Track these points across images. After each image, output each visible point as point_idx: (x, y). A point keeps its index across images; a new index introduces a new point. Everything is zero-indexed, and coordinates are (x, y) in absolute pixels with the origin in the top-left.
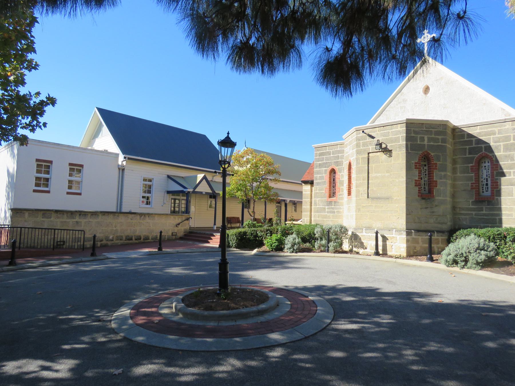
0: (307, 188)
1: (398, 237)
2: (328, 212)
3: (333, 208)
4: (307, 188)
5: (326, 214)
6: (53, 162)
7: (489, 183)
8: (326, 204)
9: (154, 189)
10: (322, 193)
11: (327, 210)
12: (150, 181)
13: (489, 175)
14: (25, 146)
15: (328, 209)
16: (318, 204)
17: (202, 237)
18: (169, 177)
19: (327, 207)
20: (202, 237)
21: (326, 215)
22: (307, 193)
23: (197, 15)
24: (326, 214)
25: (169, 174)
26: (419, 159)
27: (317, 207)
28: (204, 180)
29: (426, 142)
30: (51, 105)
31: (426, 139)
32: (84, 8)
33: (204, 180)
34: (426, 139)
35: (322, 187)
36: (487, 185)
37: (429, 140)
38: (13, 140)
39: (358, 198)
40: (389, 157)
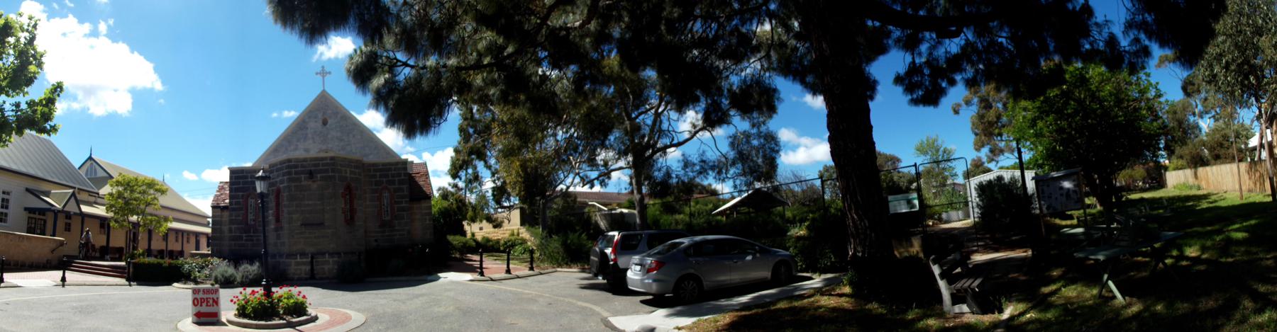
1: (331, 260)
2: (246, 240)
3: (251, 236)
6: (929, 110)
7: (389, 210)
9: (11, 205)
11: (244, 238)
12: (8, 194)
14: (35, 80)
18: (28, 190)
23: (705, 23)
25: (28, 187)
26: (609, 178)
28: (73, 198)
29: (348, 175)
31: (348, 172)
33: (73, 198)
34: (348, 172)
36: (387, 211)
37: (351, 172)
38: (1133, 61)
39: (218, 227)
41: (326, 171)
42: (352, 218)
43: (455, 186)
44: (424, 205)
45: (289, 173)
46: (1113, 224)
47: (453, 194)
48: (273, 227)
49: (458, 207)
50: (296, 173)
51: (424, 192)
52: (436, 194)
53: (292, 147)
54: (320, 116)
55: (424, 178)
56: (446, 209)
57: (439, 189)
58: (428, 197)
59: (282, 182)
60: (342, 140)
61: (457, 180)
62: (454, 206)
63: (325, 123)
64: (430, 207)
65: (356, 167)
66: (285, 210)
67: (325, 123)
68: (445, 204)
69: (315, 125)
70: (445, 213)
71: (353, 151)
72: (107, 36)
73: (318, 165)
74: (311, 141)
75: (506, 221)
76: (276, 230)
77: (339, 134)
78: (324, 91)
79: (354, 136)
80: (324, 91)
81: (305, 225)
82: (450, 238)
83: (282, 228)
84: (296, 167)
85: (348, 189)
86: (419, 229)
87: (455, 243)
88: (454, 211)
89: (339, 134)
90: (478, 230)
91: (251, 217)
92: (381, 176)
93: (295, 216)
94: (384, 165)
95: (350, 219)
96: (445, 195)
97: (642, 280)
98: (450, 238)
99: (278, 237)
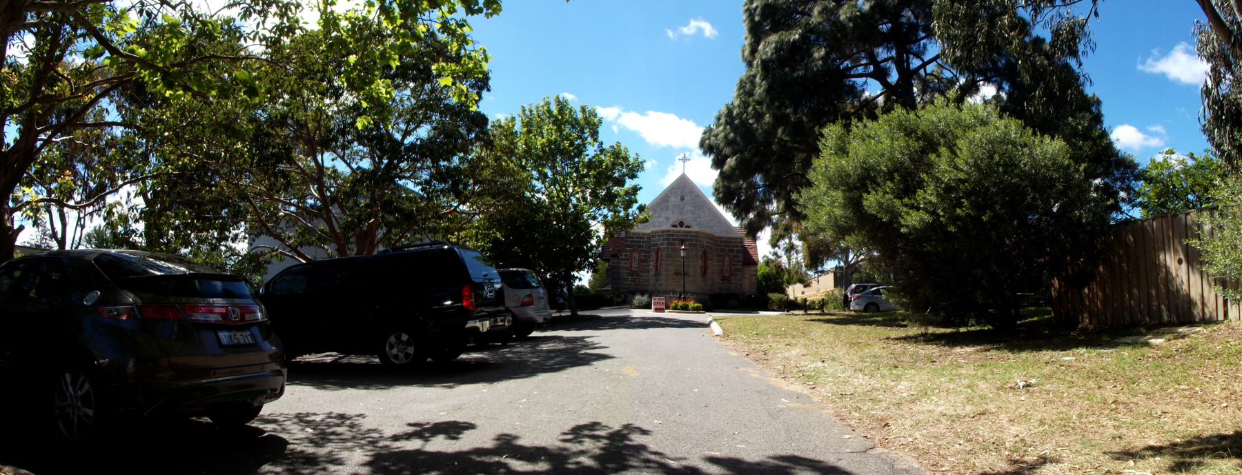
41: (692, 240)
42: (705, 272)
43: (775, 254)
44: (753, 268)
45: (668, 239)
46: (517, 253)
47: (773, 261)
48: (652, 273)
49: (777, 272)
50: (673, 240)
51: (753, 260)
52: (761, 260)
53: (657, 215)
54: (679, 193)
55: (753, 250)
56: (768, 274)
57: (764, 257)
58: (755, 263)
59: (662, 244)
60: (694, 213)
61: (777, 249)
62: (774, 271)
63: (682, 199)
64: (756, 271)
65: (710, 239)
66: (664, 263)
67: (682, 199)
68: (767, 270)
69: (674, 200)
70: (767, 277)
71: (716, 231)
72: (742, 239)
73: (687, 236)
74: (670, 212)
75: (133, 194)
76: (656, 275)
77: (692, 209)
78: (684, 174)
79: (704, 211)
80: (684, 174)
81: (677, 273)
82: (770, 295)
83: (660, 275)
84: (673, 235)
85: (705, 253)
86: (747, 285)
87: (773, 298)
88: (775, 276)
89: (692, 209)
90: (795, 292)
91: (634, 265)
92: (725, 246)
93: (670, 268)
94: (728, 238)
95: (704, 273)
96: (768, 263)
97: (741, 224)
98: (770, 295)
99: (657, 280)
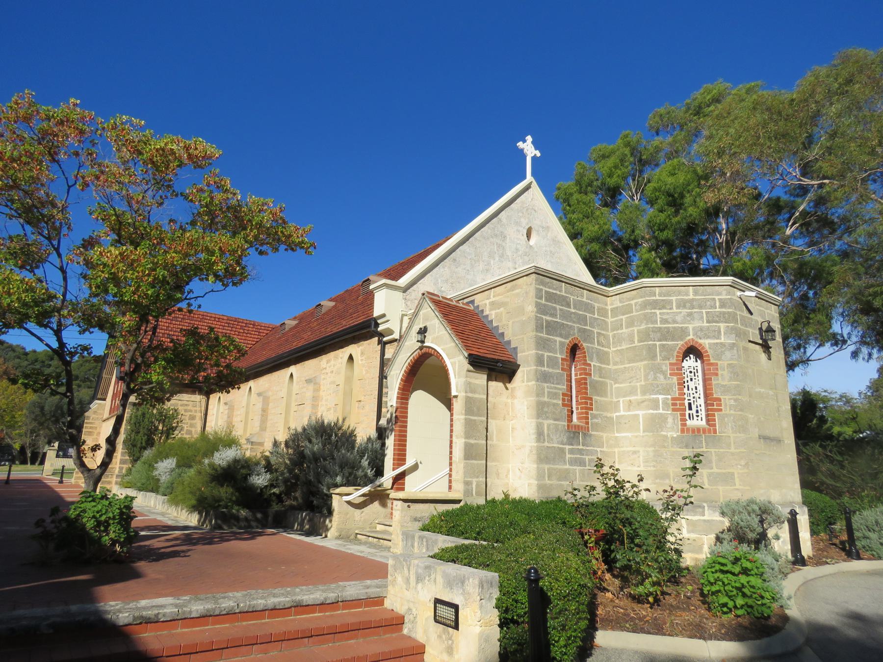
0: (478, 382)
2: (571, 464)
3: (580, 452)
4: (478, 382)
5: (567, 466)
8: (565, 440)
10: (554, 405)
11: (568, 456)
13: (749, 91)
15: (571, 452)
16: (548, 435)
17: (480, 363)
19: (567, 447)
20: (480, 363)
21: (567, 470)
22: (476, 396)
24: (567, 466)
27: (546, 444)
30: (806, 557)
32: (799, 614)
35: (556, 388)
40: (760, 329)
